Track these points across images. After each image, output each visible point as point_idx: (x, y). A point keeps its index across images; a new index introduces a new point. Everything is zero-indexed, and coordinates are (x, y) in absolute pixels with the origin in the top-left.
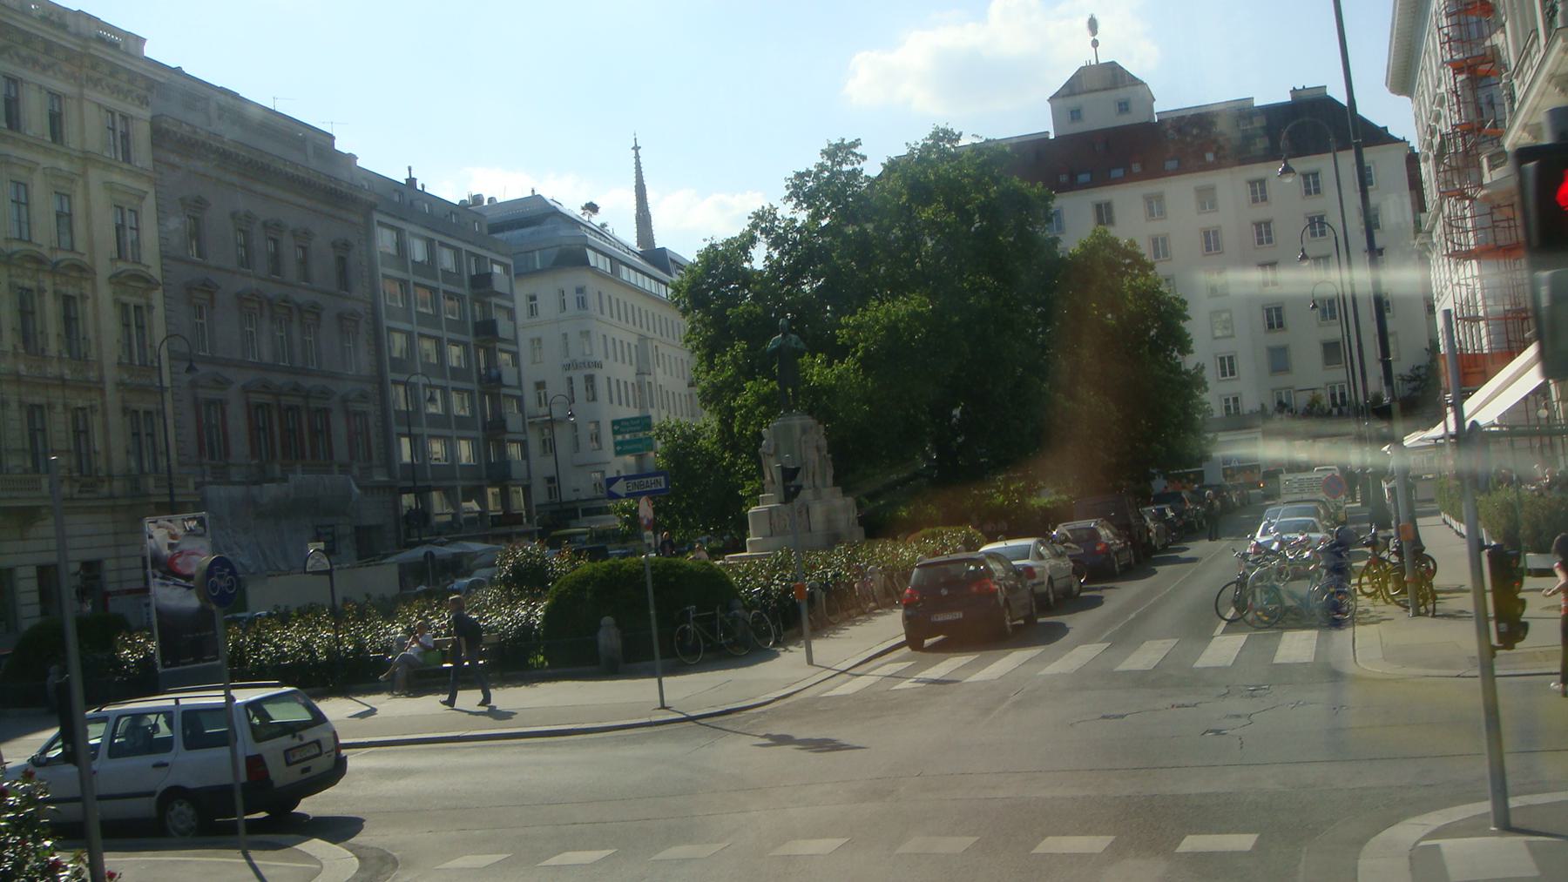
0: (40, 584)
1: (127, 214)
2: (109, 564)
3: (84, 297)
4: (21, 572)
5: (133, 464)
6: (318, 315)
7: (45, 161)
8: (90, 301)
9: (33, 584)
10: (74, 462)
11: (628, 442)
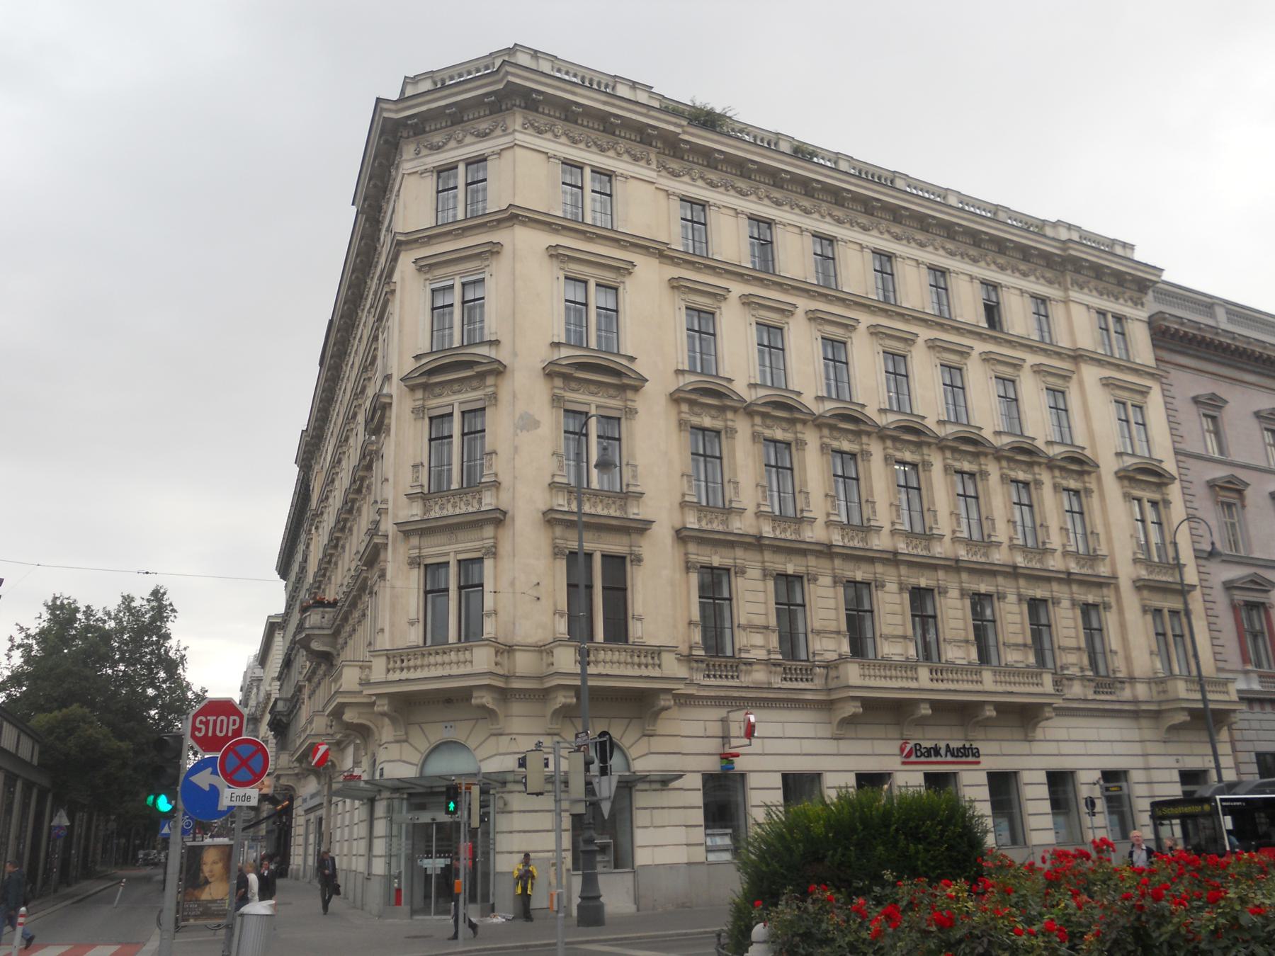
0: (1052, 792)
1: (1130, 409)
2: (1136, 776)
3: (1088, 492)
4: (1026, 777)
5: (1159, 665)
6: (1240, 492)
7: (980, 347)
8: (1095, 496)
9: (1044, 791)
10: (1086, 661)
11: (462, 439)
